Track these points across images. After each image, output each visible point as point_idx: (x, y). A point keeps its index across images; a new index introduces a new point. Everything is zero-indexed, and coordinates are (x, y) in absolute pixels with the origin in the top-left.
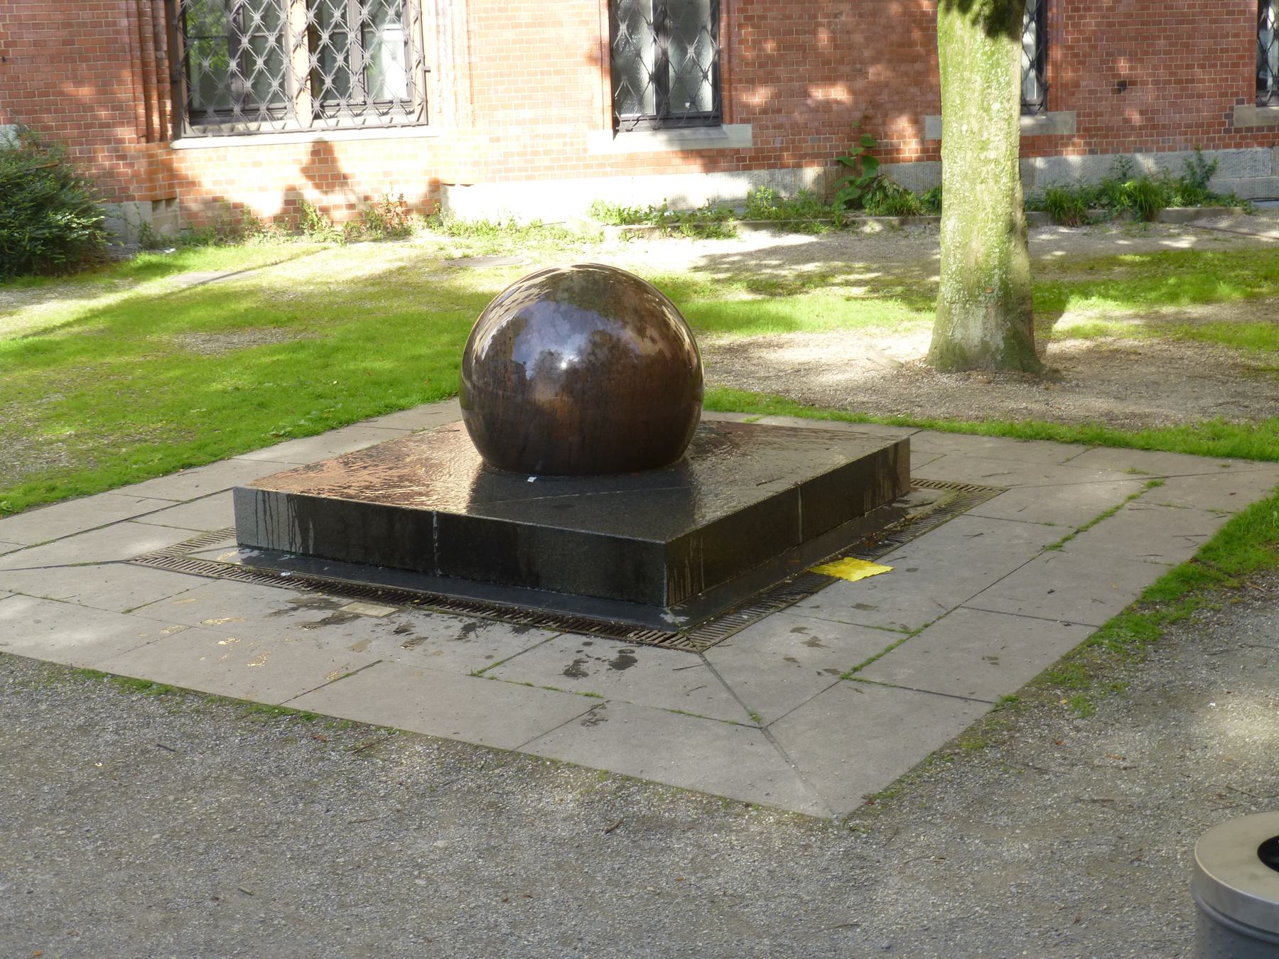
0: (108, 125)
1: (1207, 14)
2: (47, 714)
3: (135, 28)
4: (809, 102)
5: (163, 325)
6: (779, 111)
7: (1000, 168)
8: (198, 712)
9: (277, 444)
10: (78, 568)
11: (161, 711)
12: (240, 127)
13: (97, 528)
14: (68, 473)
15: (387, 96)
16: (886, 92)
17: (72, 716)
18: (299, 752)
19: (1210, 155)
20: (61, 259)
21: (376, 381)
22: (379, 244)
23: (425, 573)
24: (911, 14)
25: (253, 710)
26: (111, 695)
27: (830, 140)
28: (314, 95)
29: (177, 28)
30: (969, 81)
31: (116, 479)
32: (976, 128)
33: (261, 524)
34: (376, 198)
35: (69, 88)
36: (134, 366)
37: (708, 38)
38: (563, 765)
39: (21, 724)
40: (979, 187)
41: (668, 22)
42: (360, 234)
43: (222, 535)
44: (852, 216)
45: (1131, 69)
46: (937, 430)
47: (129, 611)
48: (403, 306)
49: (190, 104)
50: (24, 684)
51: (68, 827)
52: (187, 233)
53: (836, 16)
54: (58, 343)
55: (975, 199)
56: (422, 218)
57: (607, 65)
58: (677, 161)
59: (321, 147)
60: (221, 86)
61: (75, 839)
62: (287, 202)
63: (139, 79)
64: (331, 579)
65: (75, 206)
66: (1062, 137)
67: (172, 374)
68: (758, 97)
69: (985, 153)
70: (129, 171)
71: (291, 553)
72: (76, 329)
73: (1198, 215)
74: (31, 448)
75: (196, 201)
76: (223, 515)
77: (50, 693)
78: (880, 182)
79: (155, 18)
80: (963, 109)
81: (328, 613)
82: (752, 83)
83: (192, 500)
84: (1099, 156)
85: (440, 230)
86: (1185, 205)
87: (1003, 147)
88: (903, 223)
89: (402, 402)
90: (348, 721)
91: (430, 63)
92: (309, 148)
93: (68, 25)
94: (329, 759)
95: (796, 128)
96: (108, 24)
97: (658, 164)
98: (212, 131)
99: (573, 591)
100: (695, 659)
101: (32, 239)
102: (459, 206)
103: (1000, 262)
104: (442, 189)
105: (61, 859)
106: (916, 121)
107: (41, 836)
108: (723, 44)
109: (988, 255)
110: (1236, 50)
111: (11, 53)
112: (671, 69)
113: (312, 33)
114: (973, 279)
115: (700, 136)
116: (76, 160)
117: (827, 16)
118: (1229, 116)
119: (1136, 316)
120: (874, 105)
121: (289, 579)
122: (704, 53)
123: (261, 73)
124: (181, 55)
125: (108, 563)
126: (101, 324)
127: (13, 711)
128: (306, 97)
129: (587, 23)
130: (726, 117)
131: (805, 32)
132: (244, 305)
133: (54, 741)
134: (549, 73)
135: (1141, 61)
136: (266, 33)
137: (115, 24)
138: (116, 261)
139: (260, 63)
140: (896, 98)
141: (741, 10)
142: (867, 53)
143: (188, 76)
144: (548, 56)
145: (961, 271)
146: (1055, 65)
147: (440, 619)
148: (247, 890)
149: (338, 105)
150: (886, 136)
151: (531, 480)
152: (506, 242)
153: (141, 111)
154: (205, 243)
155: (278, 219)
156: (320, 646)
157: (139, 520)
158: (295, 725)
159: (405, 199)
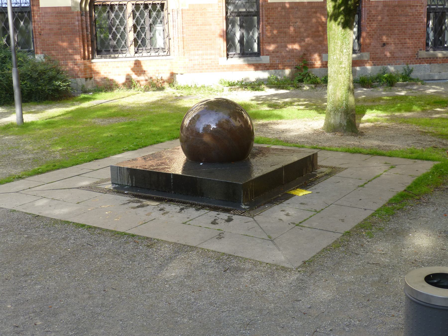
0: (72, 55)
1: (410, 23)
3: (80, 25)
4: (287, 49)
6: (278, 52)
7: (346, 70)
10: (63, 190)
12: (113, 56)
14: (60, 161)
15: (158, 47)
17: (61, 235)
18: (130, 246)
19: (411, 66)
20: (57, 96)
22: (155, 92)
24: (319, 22)
26: (73, 229)
27: (293, 61)
29: (93, 25)
30: (337, 43)
31: (74, 163)
32: (338, 57)
33: (119, 177)
34: (154, 78)
35: (60, 43)
36: (80, 128)
37: (256, 29)
40: (339, 76)
41: (244, 24)
42: (149, 89)
43: (107, 180)
44: (300, 84)
45: (387, 39)
47: (78, 203)
49: (97, 48)
50: (46, 225)
53: (295, 23)
54: (56, 121)
55: (338, 79)
56: (168, 84)
57: (225, 38)
58: (246, 67)
59: (137, 62)
61: (62, 272)
62: (127, 79)
64: (140, 194)
66: (365, 61)
67: (91, 131)
68: (272, 47)
69: (341, 65)
71: (128, 186)
72: (62, 117)
73: (407, 85)
74: (48, 153)
76: (107, 174)
78: (309, 74)
79: (86, 22)
80: (335, 52)
82: (269, 43)
83: (97, 170)
84: (376, 66)
85: (174, 88)
86: (403, 82)
87: (347, 63)
88: (315, 87)
89: (162, 140)
90: (145, 237)
91: (171, 36)
92: (134, 62)
94: (139, 248)
95: (283, 57)
96: (72, 24)
97: (240, 68)
99: (214, 198)
100: (251, 219)
102: (180, 80)
104: (174, 75)
106: (320, 56)
108: (261, 31)
109: (342, 97)
110: (419, 34)
112: (245, 39)
113: (135, 27)
114: (337, 104)
115: (254, 59)
116: (62, 65)
117: (293, 23)
118: (417, 54)
120: (307, 50)
121: (127, 194)
122: (255, 34)
123: (119, 39)
124: (94, 33)
125: (72, 188)
126: (69, 115)
127: (43, 233)
128: (133, 47)
129: (219, 24)
130: (262, 54)
131: (286, 28)
132: (113, 110)
134: (207, 40)
135: (390, 37)
136: (121, 27)
137: (74, 23)
139: (119, 36)
140: (314, 48)
141: (266, 21)
142: (305, 34)
146: (363, 38)
149: (143, 49)
150: (311, 60)
151: (201, 164)
153: (82, 50)
154: (102, 91)
155: (124, 84)
156: (136, 214)
157: (81, 175)
159: (163, 78)
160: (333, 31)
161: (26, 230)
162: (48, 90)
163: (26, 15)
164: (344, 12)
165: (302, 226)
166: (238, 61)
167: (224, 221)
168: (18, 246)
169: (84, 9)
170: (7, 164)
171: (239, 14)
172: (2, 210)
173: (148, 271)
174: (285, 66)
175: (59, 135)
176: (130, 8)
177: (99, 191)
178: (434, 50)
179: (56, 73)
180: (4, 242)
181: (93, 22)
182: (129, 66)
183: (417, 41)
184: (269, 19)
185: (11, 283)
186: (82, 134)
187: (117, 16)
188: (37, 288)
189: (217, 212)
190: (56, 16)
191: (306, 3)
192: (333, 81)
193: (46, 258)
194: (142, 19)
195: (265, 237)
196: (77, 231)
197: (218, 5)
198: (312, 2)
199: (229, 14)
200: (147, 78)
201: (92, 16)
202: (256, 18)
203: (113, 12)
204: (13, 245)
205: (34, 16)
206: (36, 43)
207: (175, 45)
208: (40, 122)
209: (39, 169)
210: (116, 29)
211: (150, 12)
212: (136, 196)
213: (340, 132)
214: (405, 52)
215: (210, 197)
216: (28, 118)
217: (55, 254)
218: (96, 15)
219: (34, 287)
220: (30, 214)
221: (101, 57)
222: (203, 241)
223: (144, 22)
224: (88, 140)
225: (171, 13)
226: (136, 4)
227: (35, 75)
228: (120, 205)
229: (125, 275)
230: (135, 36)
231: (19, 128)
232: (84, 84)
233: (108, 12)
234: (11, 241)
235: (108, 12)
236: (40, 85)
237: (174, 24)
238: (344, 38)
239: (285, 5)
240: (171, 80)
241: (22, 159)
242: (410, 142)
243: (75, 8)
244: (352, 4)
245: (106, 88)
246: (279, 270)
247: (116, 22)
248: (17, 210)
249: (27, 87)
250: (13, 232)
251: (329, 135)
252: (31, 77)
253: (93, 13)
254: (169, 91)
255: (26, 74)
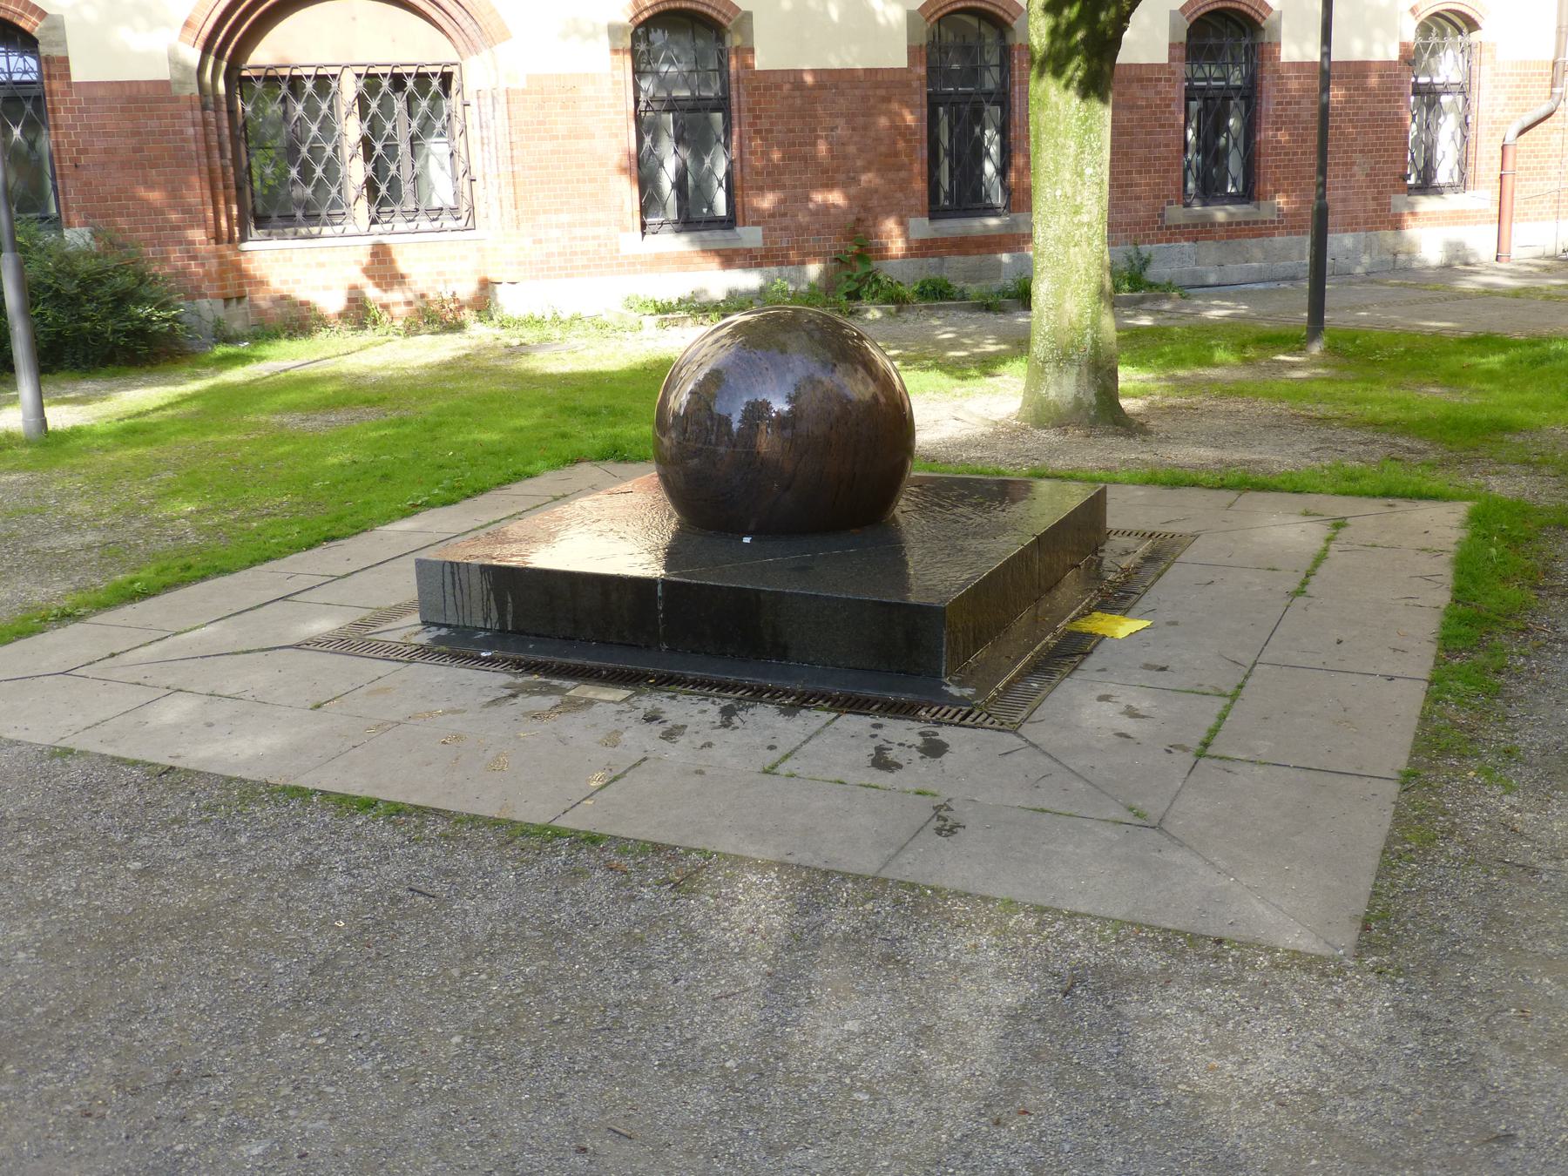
0: (179, 228)
1: (1143, 127)
2: (251, 849)
3: (201, 137)
4: (811, 206)
5: (257, 407)
6: (785, 215)
8: (446, 837)
9: (416, 513)
10: (242, 656)
11: (399, 839)
12: (303, 231)
13: (251, 609)
14: (200, 551)
15: (436, 204)
16: (875, 197)
17: (283, 851)
18: (598, 887)
19: (1146, 249)
20: (143, 350)
21: (492, 452)
23: (648, 647)
24: (897, 128)
25: (518, 832)
26: (327, 819)
27: (828, 240)
28: (371, 201)
29: (239, 138)
30: (1064, 146)
31: (256, 554)
32: (1070, 192)
33: (450, 600)
34: (431, 296)
35: (142, 192)
36: (240, 444)
37: (720, 149)
38: (949, 893)
39: (220, 867)
40: (1072, 250)
41: (686, 135)
42: (419, 328)
43: (399, 611)
44: (855, 305)
46: (1076, 480)
47: (318, 707)
48: (479, 385)
49: (254, 209)
50: (212, 809)
51: (326, 1030)
52: (257, 328)
54: (155, 425)
55: (1069, 262)
56: (474, 313)
57: (635, 174)
58: (698, 259)
60: (282, 192)
61: (342, 1051)
62: (350, 300)
63: (206, 185)
64: (541, 658)
65: (155, 300)
67: (281, 450)
68: (767, 202)
70: (201, 270)
71: (485, 629)
72: (170, 412)
73: (1142, 300)
74: (151, 525)
75: (264, 299)
76: (404, 586)
77: (247, 820)
78: (874, 276)
79: (219, 128)
81: (556, 699)
82: (761, 189)
83: (348, 575)
85: (491, 323)
87: (1096, 210)
88: (899, 310)
89: (529, 469)
90: (645, 842)
91: (475, 173)
92: (369, 250)
93: (136, 134)
94: (642, 899)
95: (802, 229)
96: (175, 133)
97: (681, 262)
98: (277, 235)
100: (1009, 740)
101: (115, 332)
102: (508, 301)
103: (1092, 322)
104: (490, 286)
105: (332, 1090)
107: (293, 1048)
109: (1081, 316)
110: (1166, 158)
111: (83, 160)
112: (690, 178)
113: (367, 144)
114: (1067, 339)
115: (718, 237)
116: (150, 260)
117: (825, 129)
118: (1161, 216)
119: (1158, 379)
120: (866, 208)
121: (491, 660)
122: (718, 163)
123: (320, 180)
124: (245, 164)
126: (194, 406)
127: (206, 848)
128: (363, 204)
129: (616, 136)
130: (740, 220)
131: (806, 144)
132: (330, 388)
133: (270, 889)
134: (584, 181)
136: (324, 144)
137: (182, 132)
138: (194, 353)
139: (319, 171)
140: (884, 203)
141: (751, 125)
142: (859, 163)
143: (251, 182)
144: (583, 166)
145: (1054, 331)
146: (1017, 171)
147: (689, 702)
148: (624, 1132)
150: (877, 236)
151: (747, 540)
152: (556, 333)
153: (210, 214)
154: (278, 337)
155: (342, 316)
156: (563, 741)
157: (295, 597)
158: (578, 851)
160: (1051, 109)
161: (130, 839)
162: (115, 332)
163: (29, 107)
164: (1086, 48)
165: (1221, 758)
166: (678, 244)
167: (916, 755)
168: (109, 916)
169: (210, 89)
170: (11, 567)
171: (672, 105)
172: (16, 752)
173: (732, 1018)
174: (808, 254)
175: (176, 466)
176: (349, 88)
177: (382, 654)
178: (1205, 204)
179: (137, 282)
180: (46, 902)
181: (242, 133)
182: (357, 262)
183: (1159, 177)
184: (759, 117)
185: (111, 1138)
186: (255, 459)
187: (312, 111)
188: (246, 1161)
189: (868, 718)
190: (123, 110)
191: (862, 73)
192: (1053, 267)
193: (249, 973)
194: (389, 119)
195: (1116, 813)
196: (348, 831)
197: (613, 76)
198: (877, 70)
199: (642, 105)
200: (410, 296)
201: (236, 111)
202: (718, 116)
203: (298, 100)
204: (86, 916)
205: (53, 111)
206: (65, 194)
207: (489, 196)
208: (100, 427)
209: (132, 582)
210: (310, 151)
211: (410, 100)
212: (530, 668)
213: (1078, 425)
214: (1129, 211)
215: (811, 659)
216: (60, 417)
217: (284, 953)
218: (248, 109)
219: (233, 1154)
220: (135, 763)
221: (269, 236)
222: (892, 851)
223: (394, 128)
224: (279, 479)
225: (474, 102)
226: (368, 76)
227: (70, 288)
228: (484, 706)
229: (642, 1046)
230: (370, 172)
231: (35, 450)
232: (222, 315)
233: (284, 99)
234: (77, 892)
235: (284, 99)
236: (86, 319)
237: (485, 134)
238: (1085, 130)
239: (802, 78)
240: (483, 302)
241: (62, 547)
242: (1304, 448)
243: (181, 83)
244: (1111, 21)
245: (288, 326)
246: (1289, 969)
247: (309, 130)
248: (78, 747)
249: (45, 325)
250: (78, 848)
251: (1049, 436)
252: (57, 294)
253: (239, 102)
254: (478, 335)
255: (40, 283)
